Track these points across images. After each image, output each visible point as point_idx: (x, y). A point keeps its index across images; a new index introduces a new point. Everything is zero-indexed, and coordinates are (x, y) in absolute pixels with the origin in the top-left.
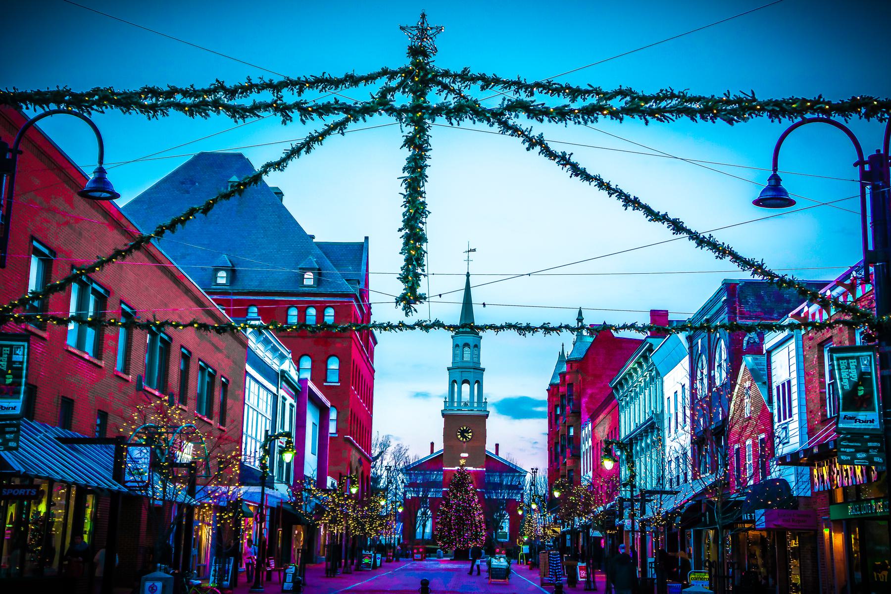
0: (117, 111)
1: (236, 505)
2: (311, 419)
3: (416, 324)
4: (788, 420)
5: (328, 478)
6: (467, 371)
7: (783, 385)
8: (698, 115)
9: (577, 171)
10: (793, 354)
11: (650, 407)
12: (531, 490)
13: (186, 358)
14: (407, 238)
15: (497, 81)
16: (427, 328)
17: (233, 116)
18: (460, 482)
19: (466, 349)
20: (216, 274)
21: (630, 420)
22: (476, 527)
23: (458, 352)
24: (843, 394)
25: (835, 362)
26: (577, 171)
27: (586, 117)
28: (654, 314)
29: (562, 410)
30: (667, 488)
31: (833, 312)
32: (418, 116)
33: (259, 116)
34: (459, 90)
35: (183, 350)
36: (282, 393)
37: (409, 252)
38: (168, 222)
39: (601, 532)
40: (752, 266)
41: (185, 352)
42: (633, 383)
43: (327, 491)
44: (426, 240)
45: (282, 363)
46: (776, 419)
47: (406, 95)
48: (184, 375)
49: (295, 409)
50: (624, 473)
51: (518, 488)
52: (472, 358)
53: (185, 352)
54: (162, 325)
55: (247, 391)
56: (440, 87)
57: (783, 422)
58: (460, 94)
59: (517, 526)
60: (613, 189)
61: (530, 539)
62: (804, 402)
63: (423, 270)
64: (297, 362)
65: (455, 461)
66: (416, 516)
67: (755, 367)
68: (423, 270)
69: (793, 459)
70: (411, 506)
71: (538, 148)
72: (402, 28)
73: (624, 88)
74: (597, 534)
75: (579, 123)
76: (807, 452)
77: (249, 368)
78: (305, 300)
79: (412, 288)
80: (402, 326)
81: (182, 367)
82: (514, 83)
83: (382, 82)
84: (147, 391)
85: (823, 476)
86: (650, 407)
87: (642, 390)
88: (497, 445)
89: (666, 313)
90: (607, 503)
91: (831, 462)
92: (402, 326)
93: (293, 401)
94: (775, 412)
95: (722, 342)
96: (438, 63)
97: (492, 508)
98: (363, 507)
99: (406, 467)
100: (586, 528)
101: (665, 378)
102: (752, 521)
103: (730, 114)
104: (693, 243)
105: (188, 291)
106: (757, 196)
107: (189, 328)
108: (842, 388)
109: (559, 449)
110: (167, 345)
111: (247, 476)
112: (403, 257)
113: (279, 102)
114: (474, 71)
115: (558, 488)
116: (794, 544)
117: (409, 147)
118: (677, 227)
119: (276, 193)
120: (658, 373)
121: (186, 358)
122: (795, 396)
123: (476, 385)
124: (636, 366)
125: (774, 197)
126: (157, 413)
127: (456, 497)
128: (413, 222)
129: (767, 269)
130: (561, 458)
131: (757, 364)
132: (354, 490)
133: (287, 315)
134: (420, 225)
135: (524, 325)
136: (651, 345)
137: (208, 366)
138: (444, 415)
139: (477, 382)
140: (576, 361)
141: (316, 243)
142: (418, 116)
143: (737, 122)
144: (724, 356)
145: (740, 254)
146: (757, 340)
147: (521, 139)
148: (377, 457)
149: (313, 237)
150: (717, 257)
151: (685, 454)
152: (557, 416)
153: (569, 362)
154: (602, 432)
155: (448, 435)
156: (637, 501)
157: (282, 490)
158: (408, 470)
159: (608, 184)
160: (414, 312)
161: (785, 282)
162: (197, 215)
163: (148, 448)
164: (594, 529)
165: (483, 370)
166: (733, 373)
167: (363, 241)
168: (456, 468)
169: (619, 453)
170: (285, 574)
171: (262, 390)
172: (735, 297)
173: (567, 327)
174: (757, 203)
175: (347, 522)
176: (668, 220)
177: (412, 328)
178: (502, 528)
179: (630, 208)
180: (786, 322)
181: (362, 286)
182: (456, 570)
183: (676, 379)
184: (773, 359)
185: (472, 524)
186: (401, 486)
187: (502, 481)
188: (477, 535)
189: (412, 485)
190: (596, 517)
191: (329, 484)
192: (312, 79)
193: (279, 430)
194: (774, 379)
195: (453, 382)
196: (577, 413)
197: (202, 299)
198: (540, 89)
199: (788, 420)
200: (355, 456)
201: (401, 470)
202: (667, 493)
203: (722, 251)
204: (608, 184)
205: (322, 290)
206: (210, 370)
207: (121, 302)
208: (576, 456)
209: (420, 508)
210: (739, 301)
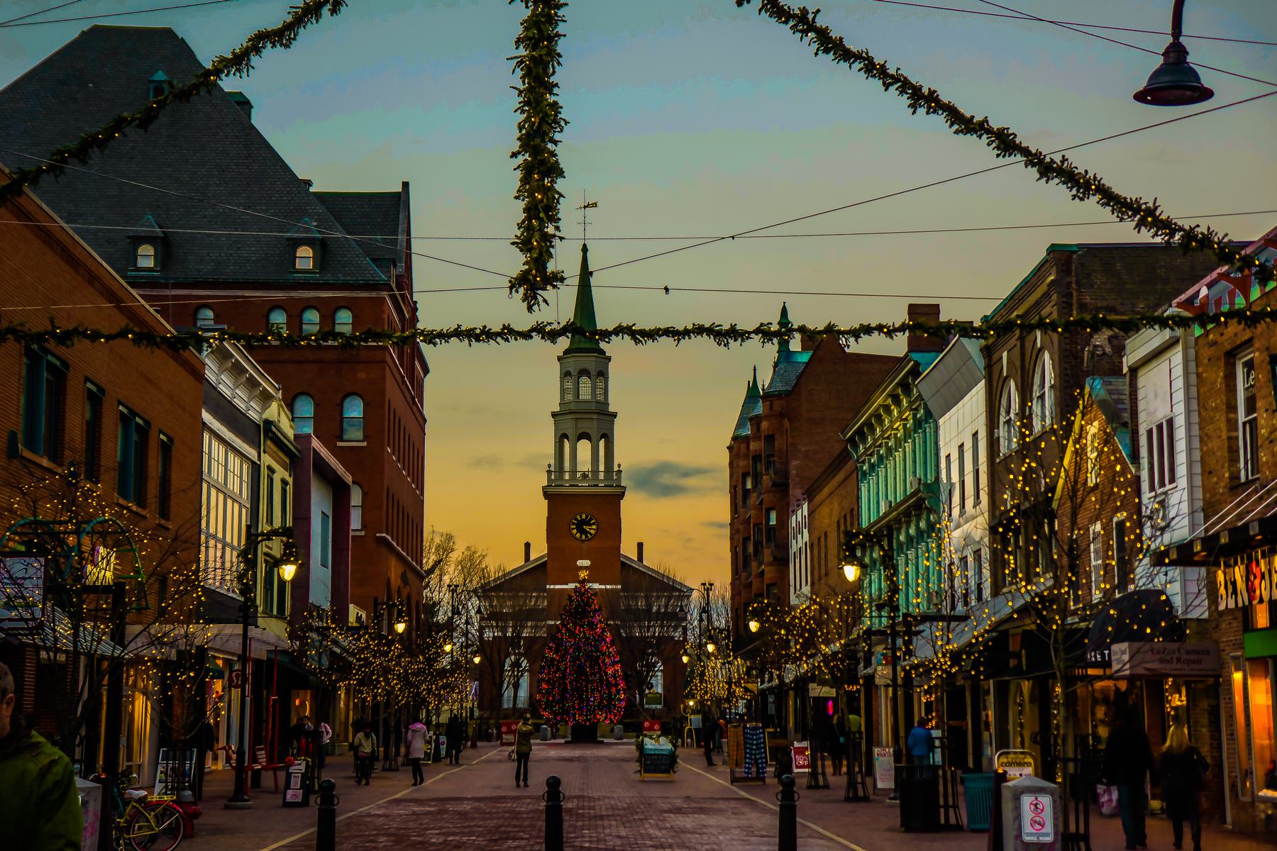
1: (198, 657)
2: (320, 503)
3: (533, 330)
5: (351, 606)
6: (587, 419)
7: (1160, 427)
10: (1178, 371)
11: (915, 472)
12: (701, 620)
13: (95, 399)
14: (528, 170)
18: (580, 607)
19: (584, 379)
20: (135, 251)
21: (877, 497)
22: (609, 685)
23: (569, 385)
28: (913, 309)
29: (756, 483)
35: (89, 385)
36: (267, 460)
37: (531, 195)
38: (73, 145)
40: (1136, 211)
44: (561, 173)
45: (264, 408)
46: (1145, 486)
49: (290, 489)
51: (678, 617)
52: (594, 393)
55: (206, 457)
59: (679, 680)
60: (892, 77)
61: (701, 703)
62: (1197, 455)
63: (557, 228)
64: (290, 404)
65: (570, 573)
66: (502, 670)
67: (1108, 397)
68: (557, 228)
69: (1183, 555)
70: (494, 652)
76: (1209, 541)
77: (206, 416)
80: (508, 333)
81: (88, 415)
85: (1234, 583)
86: (915, 472)
87: (899, 443)
88: (640, 546)
91: (1250, 559)
92: (508, 333)
93: (286, 475)
94: (1145, 475)
95: (1047, 355)
97: (636, 654)
99: (482, 587)
100: (801, 683)
101: (941, 421)
102: (1106, 664)
104: (1033, 172)
105: (93, 278)
106: (1141, 85)
107: (117, 342)
109: (751, 549)
110: (60, 375)
111: (216, 608)
112: (521, 204)
115: (757, 615)
116: (1178, 700)
118: (1006, 143)
119: (239, 103)
120: (929, 414)
121: (95, 399)
122: (1181, 446)
123: (602, 443)
124: (889, 401)
126: (57, 497)
127: (572, 635)
128: (538, 141)
129: (1163, 217)
130: (754, 564)
131: (1110, 392)
132: (400, 628)
134: (550, 146)
135: (726, 327)
137: (134, 413)
138: (546, 495)
139: (604, 436)
141: (314, 193)
145: (1117, 190)
146: (1108, 350)
148: (431, 571)
149: (308, 183)
150: (1074, 197)
151: (977, 554)
152: (746, 493)
153: (768, 396)
154: (830, 514)
157: (272, 631)
158: (486, 591)
159: (883, 66)
160: (542, 304)
161: (1195, 238)
163: (42, 560)
165: (614, 415)
166: (1066, 406)
167: (399, 189)
168: (572, 586)
170: (289, 775)
171: (231, 456)
172: (1069, 274)
174: (1140, 97)
175: (388, 682)
176: (989, 131)
177: (526, 335)
179: (922, 111)
181: (401, 269)
182: (579, 759)
183: (961, 425)
184: (1141, 381)
185: (601, 680)
186: (476, 619)
187: (650, 606)
188: (610, 700)
189: (493, 616)
191: (352, 619)
193: (264, 527)
194: (1142, 417)
195: (561, 438)
196: (781, 487)
197: (120, 293)
199: (1168, 487)
200: (394, 571)
201: (475, 591)
203: (1081, 184)
204: (883, 66)
205: (329, 278)
206: (138, 420)
208: (782, 561)
209: (508, 655)
210: (1077, 282)
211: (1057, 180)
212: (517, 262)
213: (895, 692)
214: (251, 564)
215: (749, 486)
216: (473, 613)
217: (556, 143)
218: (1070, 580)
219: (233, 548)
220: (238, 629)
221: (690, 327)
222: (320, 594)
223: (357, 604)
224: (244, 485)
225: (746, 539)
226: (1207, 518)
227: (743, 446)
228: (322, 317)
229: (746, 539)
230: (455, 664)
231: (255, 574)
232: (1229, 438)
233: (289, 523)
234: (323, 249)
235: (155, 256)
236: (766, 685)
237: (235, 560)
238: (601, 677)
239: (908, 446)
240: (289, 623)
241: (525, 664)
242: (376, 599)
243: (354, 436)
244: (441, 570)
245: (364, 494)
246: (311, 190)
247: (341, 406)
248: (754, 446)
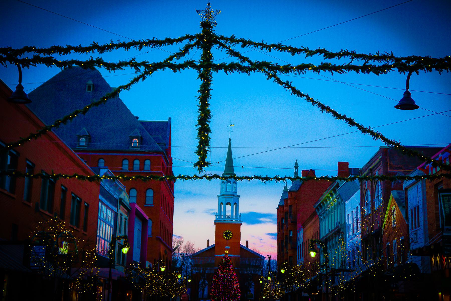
0: (44, 65)
3: (203, 176)
4: (417, 228)
5: (147, 261)
7: (415, 208)
8: (360, 70)
9: (295, 91)
10: (420, 190)
13: (64, 192)
14: (200, 130)
15: (250, 43)
16: (210, 178)
17: (108, 69)
18: (225, 263)
22: (235, 290)
24: (446, 216)
25: (441, 198)
26: (295, 91)
27: (300, 71)
28: (340, 164)
29: (286, 222)
30: (348, 268)
31: (439, 169)
32: (206, 68)
33: (122, 69)
34: (229, 46)
35: (62, 187)
39: (308, 294)
41: (64, 188)
42: (328, 206)
43: (147, 270)
47: (199, 49)
48: (63, 202)
49: (127, 221)
50: (323, 259)
53: (64, 188)
54: (57, 176)
55: (100, 211)
56: (218, 45)
57: (414, 230)
58: (229, 48)
60: (315, 102)
64: (128, 192)
68: (209, 148)
69: (419, 252)
71: (273, 79)
72: (197, 11)
73: (321, 48)
74: (306, 295)
75: (296, 74)
77: (100, 197)
78: (132, 155)
79: (203, 158)
80: (195, 177)
82: (260, 44)
83: (186, 42)
84: (41, 212)
87: (333, 210)
88: (247, 242)
89: (347, 164)
90: (312, 277)
92: (195, 177)
94: (410, 224)
96: (217, 31)
98: (167, 279)
100: (300, 291)
103: (377, 70)
104: (360, 131)
106: (397, 103)
108: (445, 213)
109: (284, 244)
112: (198, 141)
113: (133, 61)
114: (238, 37)
115: (283, 268)
117: (201, 79)
118: (351, 122)
121: (64, 192)
123: (235, 206)
124: (329, 195)
125: (407, 103)
127: (223, 273)
130: (285, 250)
132: (163, 269)
133: (122, 164)
136: (338, 184)
137: (76, 196)
139: (235, 203)
140: (294, 192)
142: (206, 68)
143: (381, 74)
144: (381, 191)
147: (264, 74)
148: (175, 249)
149: (137, 118)
152: (283, 225)
155: (218, 235)
156: (330, 275)
157: (121, 269)
162: (79, 114)
164: (305, 292)
165: (239, 197)
168: (223, 255)
169: (319, 247)
171: (108, 210)
173: (289, 178)
174: (396, 107)
175: (158, 288)
176: (346, 119)
177: (201, 178)
178: (250, 291)
180: (412, 175)
181: (167, 147)
183: (353, 204)
190: (306, 284)
192: (147, 41)
194: (409, 205)
196: (294, 223)
198: (275, 48)
199: (417, 228)
200: (162, 249)
202: (348, 271)
203: (376, 136)
206: (78, 199)
207: (27, 159)
211: (368, 134)
212: (197, 158)
214: (113, 248)
215: (284, 222)
216: (189, 264)
217: (209, 122)
218: (379, 259)
219: (108, 241)
220: (108, 269)
221: (253, 176)
222: (137, 257)
223: (149, 261)
224: (112, 220)
225: (283, 241)
226: (430, 239)
227: (282, 208)
228: (140, 162)
229: (283, 241)
230: (182, 283)
231: (114, 252)
232: (436, 213)
233: (127, 234)
234: (142, 140)
235: (86, 141)
236: (288, 292)
237: (108, 246)
238: (232, 287)
239: (336, 210)
240: (126, 268)
241: (206, 282)
242: (155, 260)
243: (150, 202)
244: (179, 249)
245: (153, 223)
246: (138, 120)
247: (146, 193)
248: (285, 208)
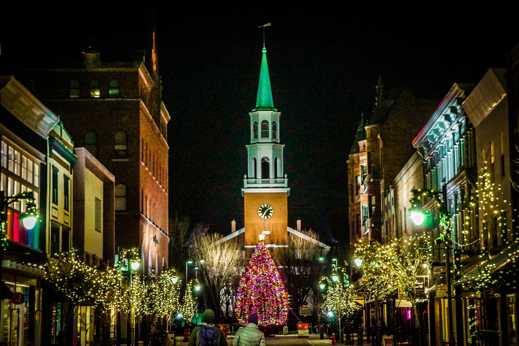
49: (70, 183)
93: (68, 173)
127: (256, 273)
188: (278, 311)
213: (450, 303)
